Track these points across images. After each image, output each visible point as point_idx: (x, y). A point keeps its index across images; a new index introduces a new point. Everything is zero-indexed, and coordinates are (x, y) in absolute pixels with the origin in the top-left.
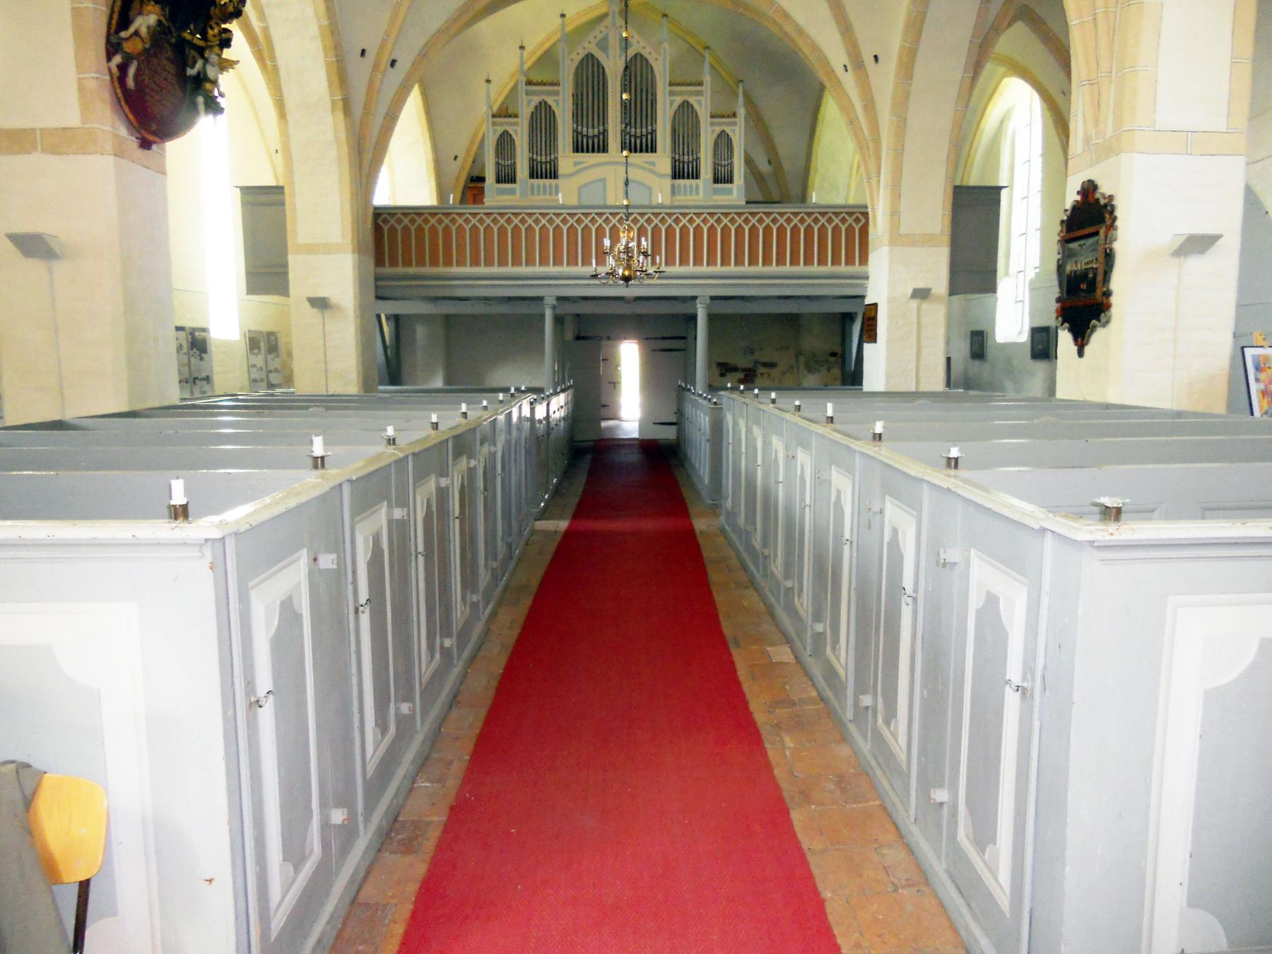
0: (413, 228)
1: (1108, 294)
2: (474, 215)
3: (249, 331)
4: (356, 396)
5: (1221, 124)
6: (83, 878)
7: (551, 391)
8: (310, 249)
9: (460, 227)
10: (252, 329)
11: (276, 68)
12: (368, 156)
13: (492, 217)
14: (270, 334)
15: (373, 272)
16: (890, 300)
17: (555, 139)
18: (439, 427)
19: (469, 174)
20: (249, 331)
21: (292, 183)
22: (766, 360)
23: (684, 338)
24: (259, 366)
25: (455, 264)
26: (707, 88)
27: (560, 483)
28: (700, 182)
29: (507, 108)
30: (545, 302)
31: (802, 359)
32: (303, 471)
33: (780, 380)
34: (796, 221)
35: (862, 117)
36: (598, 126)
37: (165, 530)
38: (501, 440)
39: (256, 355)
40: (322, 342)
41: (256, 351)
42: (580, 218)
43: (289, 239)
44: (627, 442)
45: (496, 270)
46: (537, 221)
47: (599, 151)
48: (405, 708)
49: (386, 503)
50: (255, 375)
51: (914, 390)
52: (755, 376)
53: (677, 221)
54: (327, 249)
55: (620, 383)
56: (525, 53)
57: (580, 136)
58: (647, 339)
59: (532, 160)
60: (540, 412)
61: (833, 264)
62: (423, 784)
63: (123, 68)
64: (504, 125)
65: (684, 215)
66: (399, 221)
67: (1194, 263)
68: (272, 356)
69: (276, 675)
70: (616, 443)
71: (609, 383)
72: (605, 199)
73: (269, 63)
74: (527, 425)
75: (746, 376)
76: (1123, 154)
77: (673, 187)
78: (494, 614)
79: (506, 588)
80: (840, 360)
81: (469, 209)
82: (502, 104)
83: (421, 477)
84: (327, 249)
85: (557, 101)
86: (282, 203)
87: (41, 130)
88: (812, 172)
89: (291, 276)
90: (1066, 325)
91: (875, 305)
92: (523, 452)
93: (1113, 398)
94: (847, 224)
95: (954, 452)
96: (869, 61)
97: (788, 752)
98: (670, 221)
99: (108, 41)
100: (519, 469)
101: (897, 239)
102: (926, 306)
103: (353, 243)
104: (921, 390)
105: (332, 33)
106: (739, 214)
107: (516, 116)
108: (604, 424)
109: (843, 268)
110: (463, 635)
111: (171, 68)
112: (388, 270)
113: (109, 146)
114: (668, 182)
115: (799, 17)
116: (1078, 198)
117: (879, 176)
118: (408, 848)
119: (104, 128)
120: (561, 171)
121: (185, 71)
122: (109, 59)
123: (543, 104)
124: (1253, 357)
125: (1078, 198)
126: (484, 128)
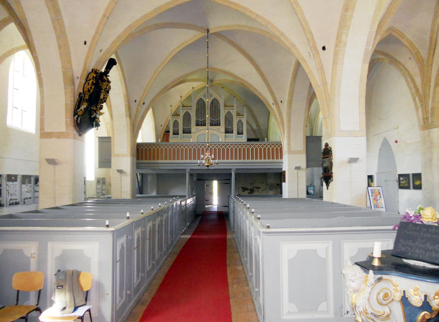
1: (332, 173)
2: (166, 145)
3: (97, 178)
4: (129, 199)
5: (358, 129)
6: (87, 290)
7: (188, 197)
8: (118, 156)
9: (162, 149)
10: (98, 177)
11: (111, 106)
12: (136, 129)
14: (103, 178)
15: (136, 162)
16: (289, 170)
17: (191, 119)
19: (166, 130)
20: (97, 178)
21: (114, 136)
22: (257, 186)
23: (229, 180)
24: (99, 188)
26: (235, 108)
27: (190, 225)
29: (177, 113)
31: (268, 186)
32: (125, 219)
33: (261, 193)
37: (105, 229)
38: (170, 212)
39: (99, 185)
40: (120, 183)
41: (99, 184)
43: (112, 152)
44: (213, 212)
45: (172, 161)
46: (184, 147)
48: (143, 275)
49: (141, 227)
50: (98, 191)
51: (297, 197)
53: (225, 147)
55: (213, 193)
56: (182, 98)
58: (220, 180)
59: (183, 128)
60: (183, 203)
62: (146, 294)
63: (77, 118)
64: (176, 118)
66: (144, 147)
67: (354, 165)
68: (103, 185)
71: (210, 193)
72: (205, 141)
73: (109, 104)
74: (178, 208)
76: (333, 137)
77: (225, 136)
78: (166, 259)
80: (280, 186)
81: (165, 143)
83: (149, 221)
87: (55, 132)
89: (112, 163)
90: (324, 181)
91: (285, 171)
93: (335, 201)
95: (259, 216)
96: (280, 103)
98: (223, 147)
100: (176, 219)
102: (299, 171)
104: (299, 197)
105: (127, 96)
108: (206, 206)
109: (275, 160)
110: (158, 262)
111: (88, 116)
112: (140, 161)
113: (72, 137)
114: (224, 134)
115: (260, 90)
118: (143, 304)
120: (192, 131)
121: (91, 116)
122: (74, 116)
123: (187, 112)
125: (325, 147)
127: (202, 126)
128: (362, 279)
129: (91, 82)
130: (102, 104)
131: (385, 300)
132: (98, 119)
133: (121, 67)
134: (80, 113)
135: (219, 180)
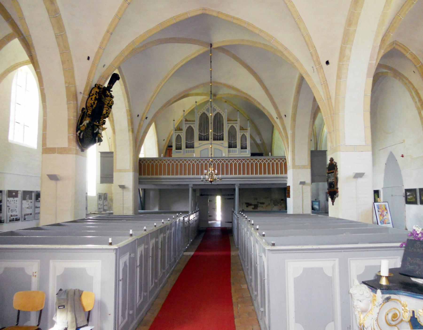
0: (151, 164)
1: (337, 189)
4: (132, 216)
5: (364, 143)
7: (191, 213)
8: (120, 171)
12: (138, 143)
13: (174, 161)
14: (105, 194)
16: (293, 185)
18: (156, 226)
19: (168, 144)
24: (101, 204)
25: (163, 175)
28: (237, 149)
30: (189, 186)
34: (265, 161)
35: (282, 131)
36: (206, 133)
38: (173, 229)
41: (101, 199)
42: (200, 161)
47: (206, 140)
48: (145, 294)
49: (143, 244)
50: (100, 207)
51: (302, 213)
52: (258, 207)
54: (125, 171)
55: (216, 208)
56: (185, 112)
57: (201, 136)
58: (223, 195)
59: (186, 143)
61: (277, 174)
63: (80, 134)
64: (179, 133)
65: (231, 160)
66: (146, 162)
68: (105, 201)
69: (123, 276)
70: (214, 228)
71: (213, 208)
75: (255, 207)
77: (229, 150)
79: (173, 270)
81: (167, 159)
82: (178, 125)
83: (152, 238)
84: (125, 171)
85: (194, 126)
86: (113, 157)
88: (273, 144)
89: (114, 178)
92: (180, 232)
94: (280, 162)
95: (264, 233)
96: (283, 117)
97: (238, 308)
99: (77, 128)
101: (294, 167)
102: (304, 187)
103: (133, 169)
104: (304, 213)
105: (130, 111)
106: (248, 159)
107: (182, 130)
108: (210, 222)
109: (279, 175)
112: (143, 176)
113: (75, 152)
114: (227, 149)
116: (330, 162)
117: (288, 148)
118: (145, 325)
119: (73, 148)
120: (195, 146)
122: (77, 132)
124: (377, 205)
125: (330, 162)
126: (172, 132)
127: (205, 140)
128: (370, 299)
129: (94, 97)
130: (105, 119)
131: (393, 321)
132: (101, 134)
133: (124, 82)
134: (83, 128)
135: (223, 196)
